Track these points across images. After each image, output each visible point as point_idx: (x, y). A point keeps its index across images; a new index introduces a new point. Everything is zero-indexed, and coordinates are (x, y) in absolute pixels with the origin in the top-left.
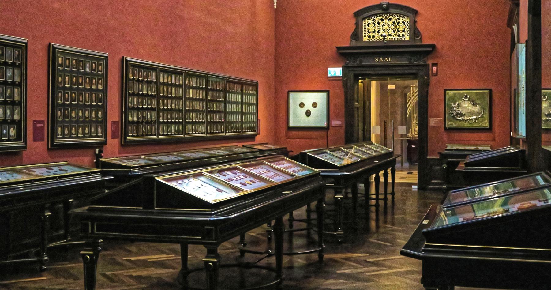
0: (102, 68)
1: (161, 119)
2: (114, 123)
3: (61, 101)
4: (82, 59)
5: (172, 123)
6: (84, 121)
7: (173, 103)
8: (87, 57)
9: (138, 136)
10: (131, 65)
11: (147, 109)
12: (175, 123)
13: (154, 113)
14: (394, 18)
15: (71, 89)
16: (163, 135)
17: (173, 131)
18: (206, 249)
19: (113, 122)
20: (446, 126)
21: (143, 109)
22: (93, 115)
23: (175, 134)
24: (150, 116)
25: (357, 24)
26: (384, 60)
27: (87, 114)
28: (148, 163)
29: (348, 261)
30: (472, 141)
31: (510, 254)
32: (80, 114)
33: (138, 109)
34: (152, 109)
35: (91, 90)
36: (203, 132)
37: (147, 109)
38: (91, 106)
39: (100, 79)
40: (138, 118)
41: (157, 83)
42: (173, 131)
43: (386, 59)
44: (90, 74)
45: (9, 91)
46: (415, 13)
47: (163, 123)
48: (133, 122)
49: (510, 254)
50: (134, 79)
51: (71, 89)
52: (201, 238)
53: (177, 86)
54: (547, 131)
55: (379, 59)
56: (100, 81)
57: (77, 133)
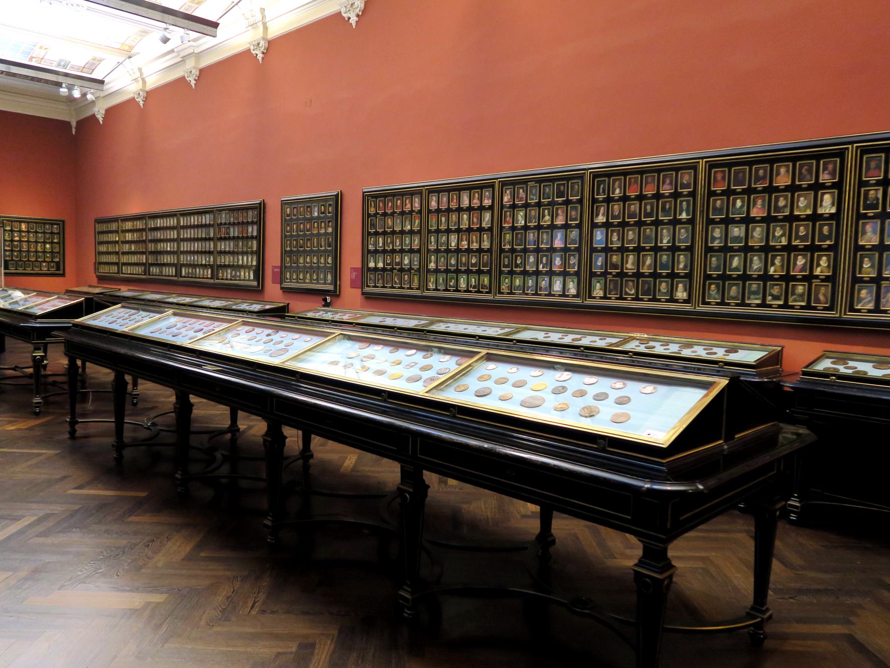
0: (333, 209)
2: (354, 269)
3: (510, 246)
4: (309, 205)
6: (311, 267)
8: (311, 200)
9: (384, 287)
10: (371, 197)
11: (402, 251)
15: (298, 235)
16: (436, 289)
18: (641, 545)
19: (351, 268)
20: (693, 173)
21: (393, 251)
22: (322, 260)
23: (231, 280)
27: (315, 260)
28: (438, 326)
29: (298, 647)
30: (12, 100)
32: (308, 260)
33: (384, 252)
35: (319, 235)
37: (402, 251)
38: (318, 251)
39: (329, 222)
41: (425, 212)
44: (318, 218)
45: (250, 243)
48: (376, 269)
50: (377, 214)
51: (298, 235)
52: (629, 517)
54: (887, 279)
56: (330, 224)
57: (305, 278)
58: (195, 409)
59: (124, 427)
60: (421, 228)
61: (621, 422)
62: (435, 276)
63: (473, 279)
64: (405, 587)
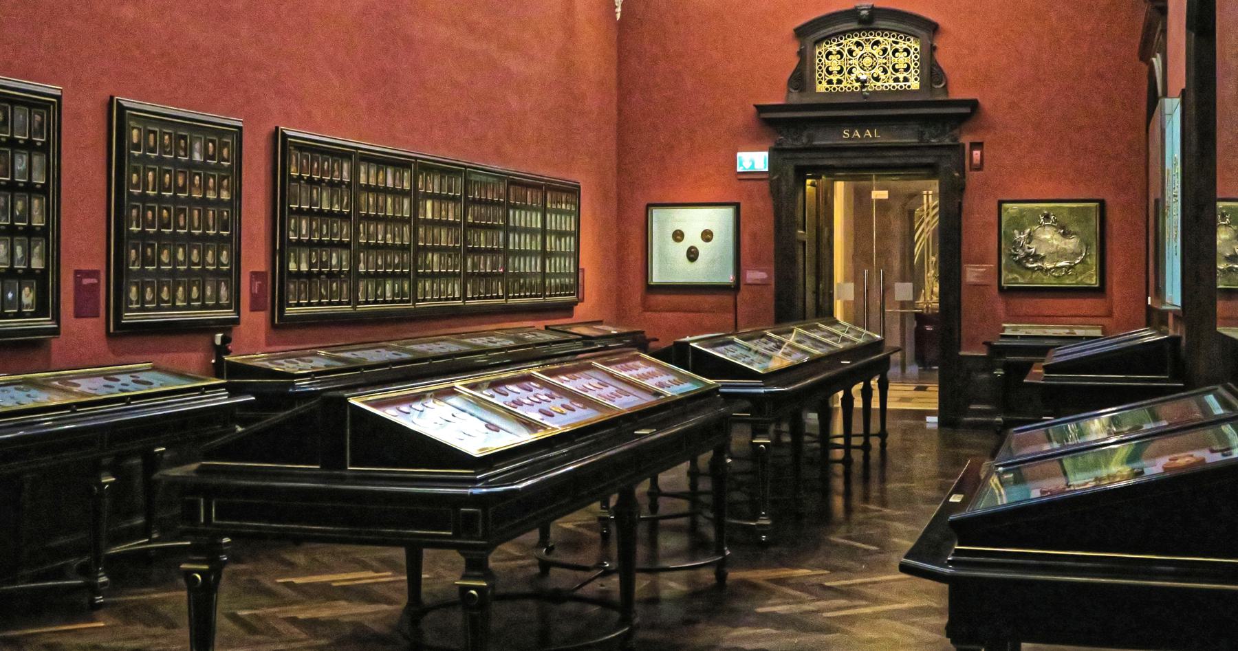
0: (230, 153)
1: (362, 268)
2: (255, 275)
4: (184, 134)
5: (385, 276)
6: (189, 272)
7: (389, 231)
8: (196, 128)
9: (309, 304)
10: (295, 147)
11: (331, 244)
12: (393, 276)
13: (345, 255)
14: (886, 41)
15: (159, 199)
16: (367, 302)
17: (388, 294)
18: (462, 559)
19: (253, 273)
21: (321, 244)
22: (210, 257)
23: (393, 301)
24: (336, 260)
25: (801, 54)
26: (862, 134)
27: (195, 257)
31: (1146, 569)
32: (180, 256)
33: (310, 244)
34: (342, 245)
35: (205, 202)
36: (457, 295)
37: (331, 244)
38: (204, 238)
39: (224, 178)
40: (311, 265)
41: (354, 187)
42: (388, 294)
43: (868, 133)
44: (203, 166)
45: (20, 205)
46: (933, 28)
47: (367, 275)
48: (299, 274)
49: (1146, 569)
50: (300, 177)
51: (159, 199)
52: (451, 533)
53: (397, 193)
55: (851, 133)
56: (225, 182)
57: (174, 297)
58: (935, 423)
59: (937, 405)
60: (411, 243)
61: (509, 432)
62: (25, 157)
63: (211, 212)
64: (761, 518)
